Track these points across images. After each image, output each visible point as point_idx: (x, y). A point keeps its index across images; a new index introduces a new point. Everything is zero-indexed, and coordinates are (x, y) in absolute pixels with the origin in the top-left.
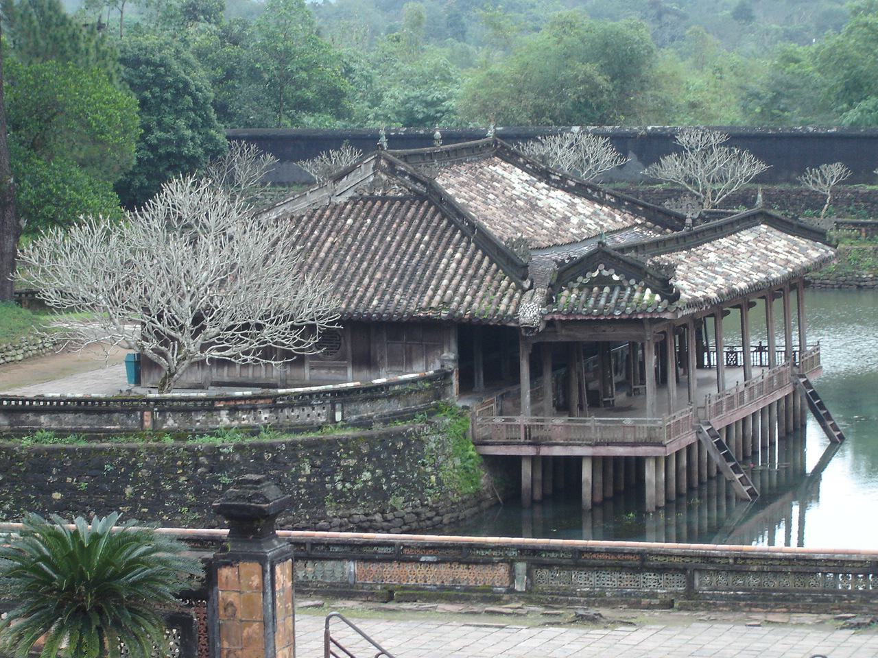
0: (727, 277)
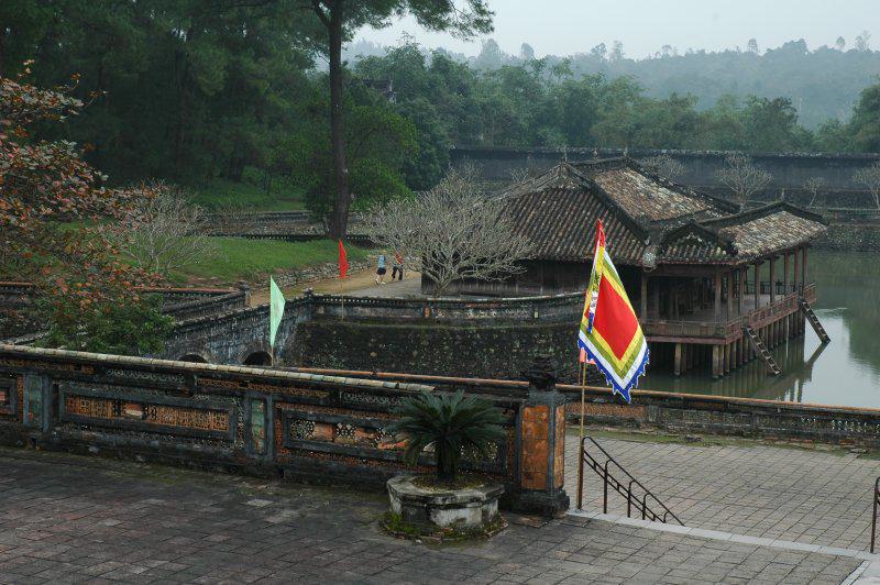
0: (764, 241)
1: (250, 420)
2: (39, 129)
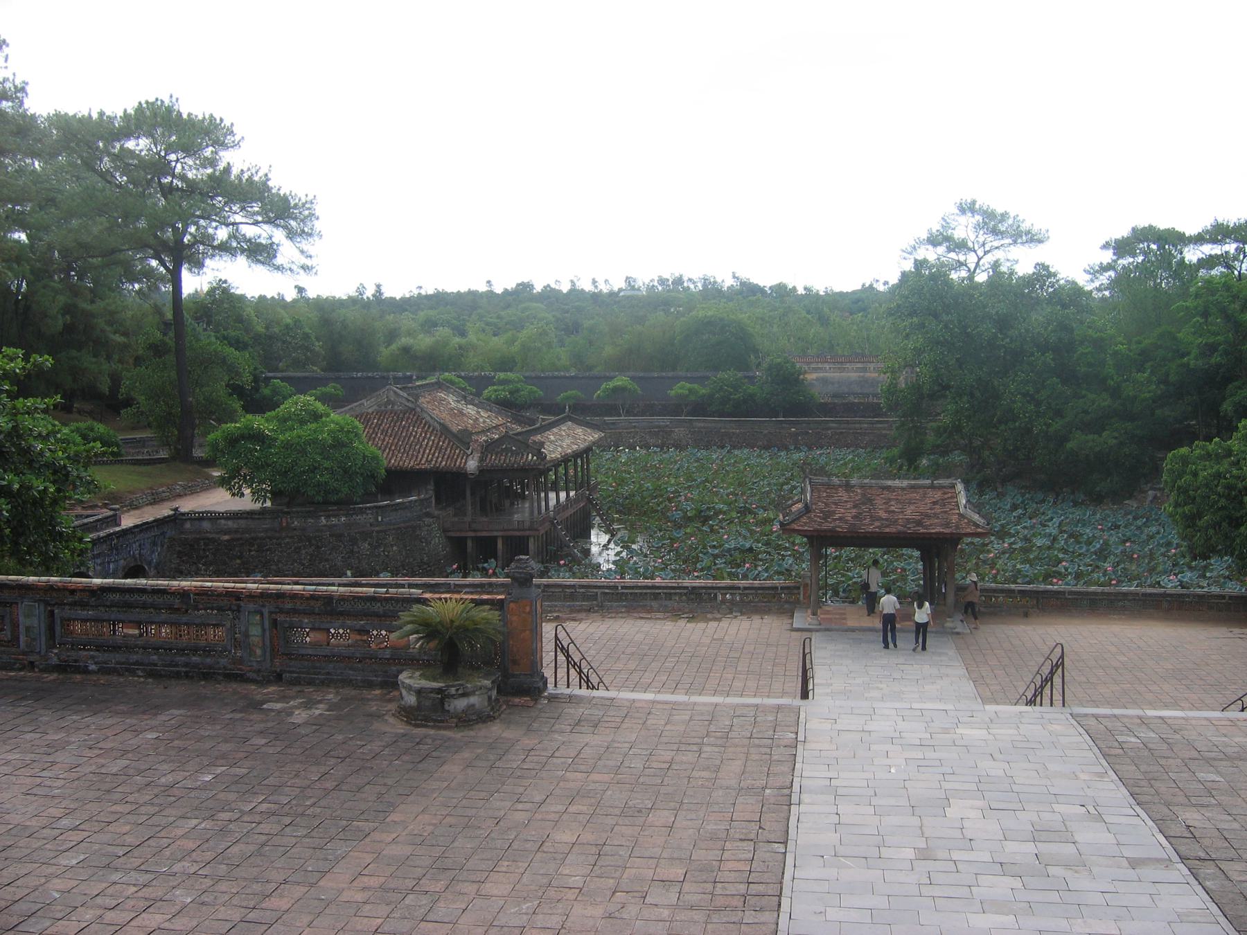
1: (247, 630)
2: (24, 386)
